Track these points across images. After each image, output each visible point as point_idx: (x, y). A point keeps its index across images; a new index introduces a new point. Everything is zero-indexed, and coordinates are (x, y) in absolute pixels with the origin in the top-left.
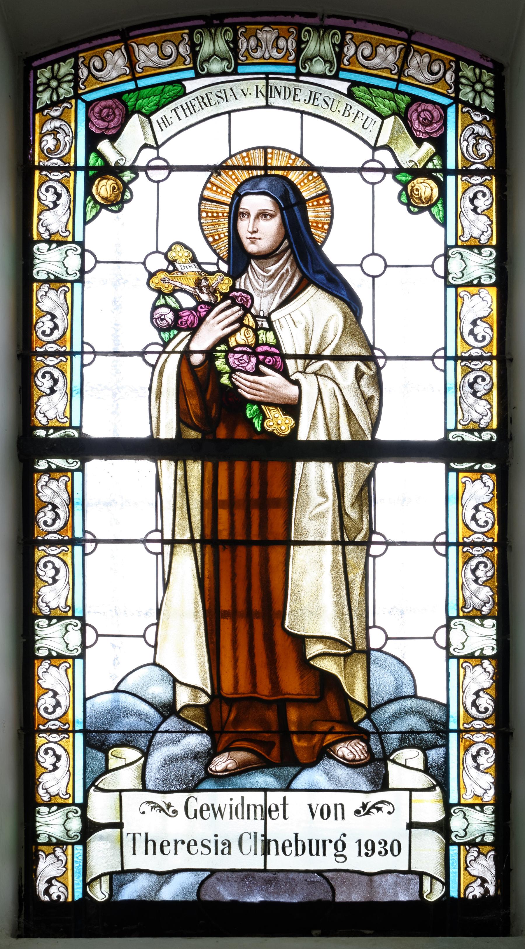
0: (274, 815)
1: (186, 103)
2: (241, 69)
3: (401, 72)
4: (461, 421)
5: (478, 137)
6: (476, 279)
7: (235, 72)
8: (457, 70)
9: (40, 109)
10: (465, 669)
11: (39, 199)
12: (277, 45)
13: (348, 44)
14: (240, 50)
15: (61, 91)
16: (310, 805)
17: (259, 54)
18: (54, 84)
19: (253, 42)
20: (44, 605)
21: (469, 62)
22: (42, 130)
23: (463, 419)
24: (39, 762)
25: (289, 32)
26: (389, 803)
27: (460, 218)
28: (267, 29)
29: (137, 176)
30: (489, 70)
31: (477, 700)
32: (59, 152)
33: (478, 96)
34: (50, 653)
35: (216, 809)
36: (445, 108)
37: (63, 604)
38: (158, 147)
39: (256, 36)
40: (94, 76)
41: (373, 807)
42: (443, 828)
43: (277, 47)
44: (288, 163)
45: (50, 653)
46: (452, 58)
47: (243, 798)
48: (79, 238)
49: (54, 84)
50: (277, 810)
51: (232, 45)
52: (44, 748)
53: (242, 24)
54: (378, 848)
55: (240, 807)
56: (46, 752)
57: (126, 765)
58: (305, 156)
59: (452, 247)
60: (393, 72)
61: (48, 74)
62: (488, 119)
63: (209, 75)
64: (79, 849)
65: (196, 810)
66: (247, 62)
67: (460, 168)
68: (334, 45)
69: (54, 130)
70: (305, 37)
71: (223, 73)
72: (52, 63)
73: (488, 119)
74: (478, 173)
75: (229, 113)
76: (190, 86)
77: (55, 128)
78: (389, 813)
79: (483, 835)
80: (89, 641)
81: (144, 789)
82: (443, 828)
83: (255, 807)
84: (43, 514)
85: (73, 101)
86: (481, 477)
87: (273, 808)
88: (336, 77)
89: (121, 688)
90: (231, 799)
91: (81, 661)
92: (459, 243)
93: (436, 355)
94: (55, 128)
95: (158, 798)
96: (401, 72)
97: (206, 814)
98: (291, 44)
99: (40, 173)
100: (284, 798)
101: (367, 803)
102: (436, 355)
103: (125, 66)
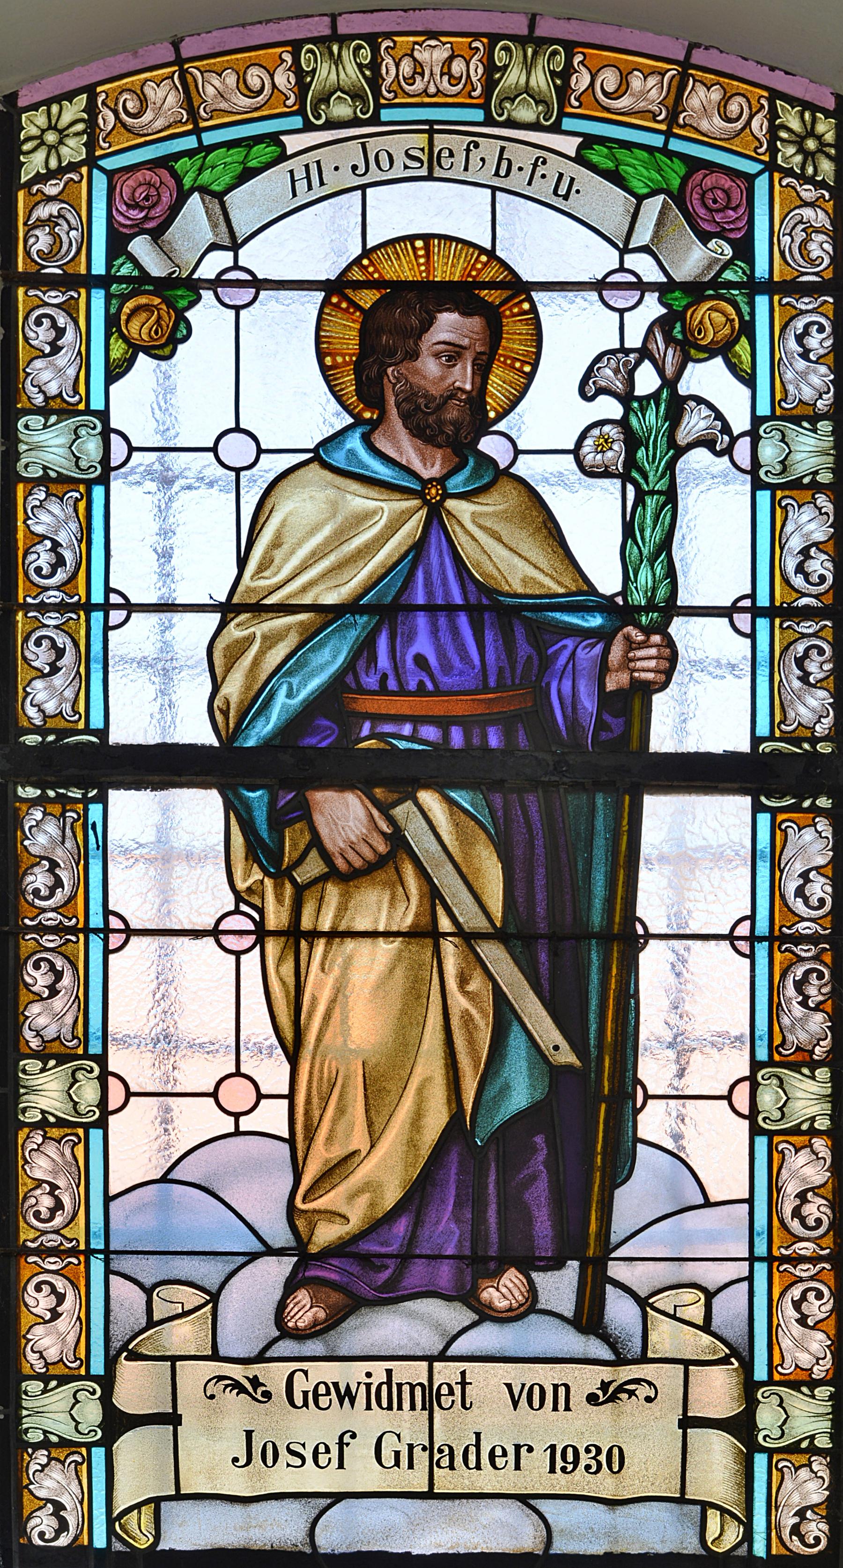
0: (446, 1401)
2: (386, 115)
3: (672, 119)
4: (779, 1368)
5: (810, 230)
6: (806, 1120)
7: (375, 120)
8: (773, 114)
9: (26, 182)
10: (785, 831)
11: (26, 339)
12: (449, 68)
13: (577, 72)
14: (384, 80)
15: (64, 150)
16: (509, 1386)
17: (419, 85)
18: (51, 138)
19: (406, 67)
20: (36, 390)
21: (792, 101)
22: (28, 220)
23: (781, 1365)
24: (26, 1305)
25: (471, 49)
26: (650, 1383)
27: (778, 1017)
28: (433, 43)
29: (199, 298)
30: (827, 114)
31: (806, 564)
32: (58, 257)
33: (810, 161)
34: (46, 474)
36: (750, 179)
37: (66, 1032)
38: (235, 246)
39: (411, 55)
40: (124, 125)
41: (620, 1389)
42: (742, 1427)
43: (451, 76)
44: (469, 275)
45: (46, 474)
46: (765, 94)
47: (389, 1372)
48: (97, 403)
49: (51, 138)
50: (451, 1392)
51: (368, 73)
52: (36, 1280)
53: (388, 35)
54: (584, 1459)
55: (384, 1388)
56: (38, 1288)
57: (185, 1314)
59: (765, 419)
60: (659, 118)
61: (41, 119)
62: (827, 198)
63: (331, 125)
64: (99, 1453)
66: (397, 101)
67: (778, 604)
68: (553, 74)
69: (49, 220)
70: (500, 60)
71: (355, 122)
72: (48, 103)
73: (827, 198)
74: (807, 613)
75: (363, 188)
76: (293, 143)
77: (51, 216)
78: (649, 1399)
79: (816, 473)
80: (117, 457)
81: (215, 1356)
82: (742, 1427)
83: (412, 1387)
84: (35, 556)
85: (84, 170)
86: (813, 497)
87: (445, 1390)
88: (555, 128)
89: (173, 1175)
90: (369, 1375)
91: (100, 1132)
92: (777, 1377)
94: (51, 216)
95: (236, 1372)
96: (672, 119)
97: (324, 1401)
98: (477, 71)
99: (25, 615)
100: (463, 1374)
101: (611, 1382)
103: (181, 107)
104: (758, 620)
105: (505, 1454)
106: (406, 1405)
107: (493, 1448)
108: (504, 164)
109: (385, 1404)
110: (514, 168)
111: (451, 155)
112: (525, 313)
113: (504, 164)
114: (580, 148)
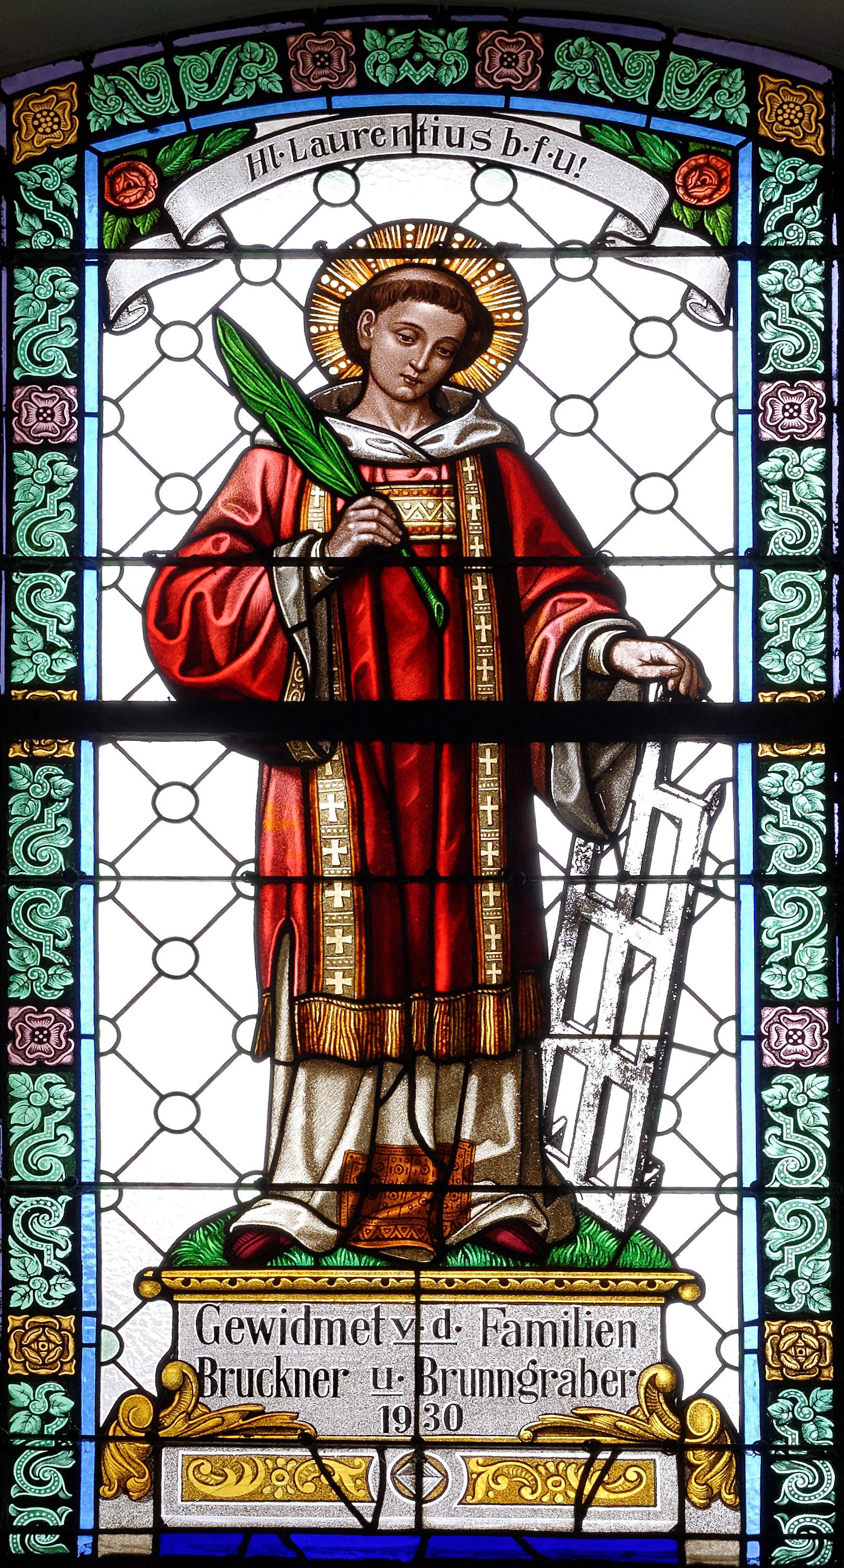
1: (345, 134)
35: (257, 1327)
55: (302, 1325)
58: (531, 311)
65: (217, 1329)
83: (542, 1326)
93: (721, 873)
97: (236, 1334)
102: (721, 873)
104: (741, 571)
105: (611, 1329)
106: (560, 1342)
107: (356, 1322)
108: (513, 145)
109: (302, 1339)
110: (522, 148)
111: (383, 133)
112: (318, 325)
113: (513, 145)
114: (254, 130)
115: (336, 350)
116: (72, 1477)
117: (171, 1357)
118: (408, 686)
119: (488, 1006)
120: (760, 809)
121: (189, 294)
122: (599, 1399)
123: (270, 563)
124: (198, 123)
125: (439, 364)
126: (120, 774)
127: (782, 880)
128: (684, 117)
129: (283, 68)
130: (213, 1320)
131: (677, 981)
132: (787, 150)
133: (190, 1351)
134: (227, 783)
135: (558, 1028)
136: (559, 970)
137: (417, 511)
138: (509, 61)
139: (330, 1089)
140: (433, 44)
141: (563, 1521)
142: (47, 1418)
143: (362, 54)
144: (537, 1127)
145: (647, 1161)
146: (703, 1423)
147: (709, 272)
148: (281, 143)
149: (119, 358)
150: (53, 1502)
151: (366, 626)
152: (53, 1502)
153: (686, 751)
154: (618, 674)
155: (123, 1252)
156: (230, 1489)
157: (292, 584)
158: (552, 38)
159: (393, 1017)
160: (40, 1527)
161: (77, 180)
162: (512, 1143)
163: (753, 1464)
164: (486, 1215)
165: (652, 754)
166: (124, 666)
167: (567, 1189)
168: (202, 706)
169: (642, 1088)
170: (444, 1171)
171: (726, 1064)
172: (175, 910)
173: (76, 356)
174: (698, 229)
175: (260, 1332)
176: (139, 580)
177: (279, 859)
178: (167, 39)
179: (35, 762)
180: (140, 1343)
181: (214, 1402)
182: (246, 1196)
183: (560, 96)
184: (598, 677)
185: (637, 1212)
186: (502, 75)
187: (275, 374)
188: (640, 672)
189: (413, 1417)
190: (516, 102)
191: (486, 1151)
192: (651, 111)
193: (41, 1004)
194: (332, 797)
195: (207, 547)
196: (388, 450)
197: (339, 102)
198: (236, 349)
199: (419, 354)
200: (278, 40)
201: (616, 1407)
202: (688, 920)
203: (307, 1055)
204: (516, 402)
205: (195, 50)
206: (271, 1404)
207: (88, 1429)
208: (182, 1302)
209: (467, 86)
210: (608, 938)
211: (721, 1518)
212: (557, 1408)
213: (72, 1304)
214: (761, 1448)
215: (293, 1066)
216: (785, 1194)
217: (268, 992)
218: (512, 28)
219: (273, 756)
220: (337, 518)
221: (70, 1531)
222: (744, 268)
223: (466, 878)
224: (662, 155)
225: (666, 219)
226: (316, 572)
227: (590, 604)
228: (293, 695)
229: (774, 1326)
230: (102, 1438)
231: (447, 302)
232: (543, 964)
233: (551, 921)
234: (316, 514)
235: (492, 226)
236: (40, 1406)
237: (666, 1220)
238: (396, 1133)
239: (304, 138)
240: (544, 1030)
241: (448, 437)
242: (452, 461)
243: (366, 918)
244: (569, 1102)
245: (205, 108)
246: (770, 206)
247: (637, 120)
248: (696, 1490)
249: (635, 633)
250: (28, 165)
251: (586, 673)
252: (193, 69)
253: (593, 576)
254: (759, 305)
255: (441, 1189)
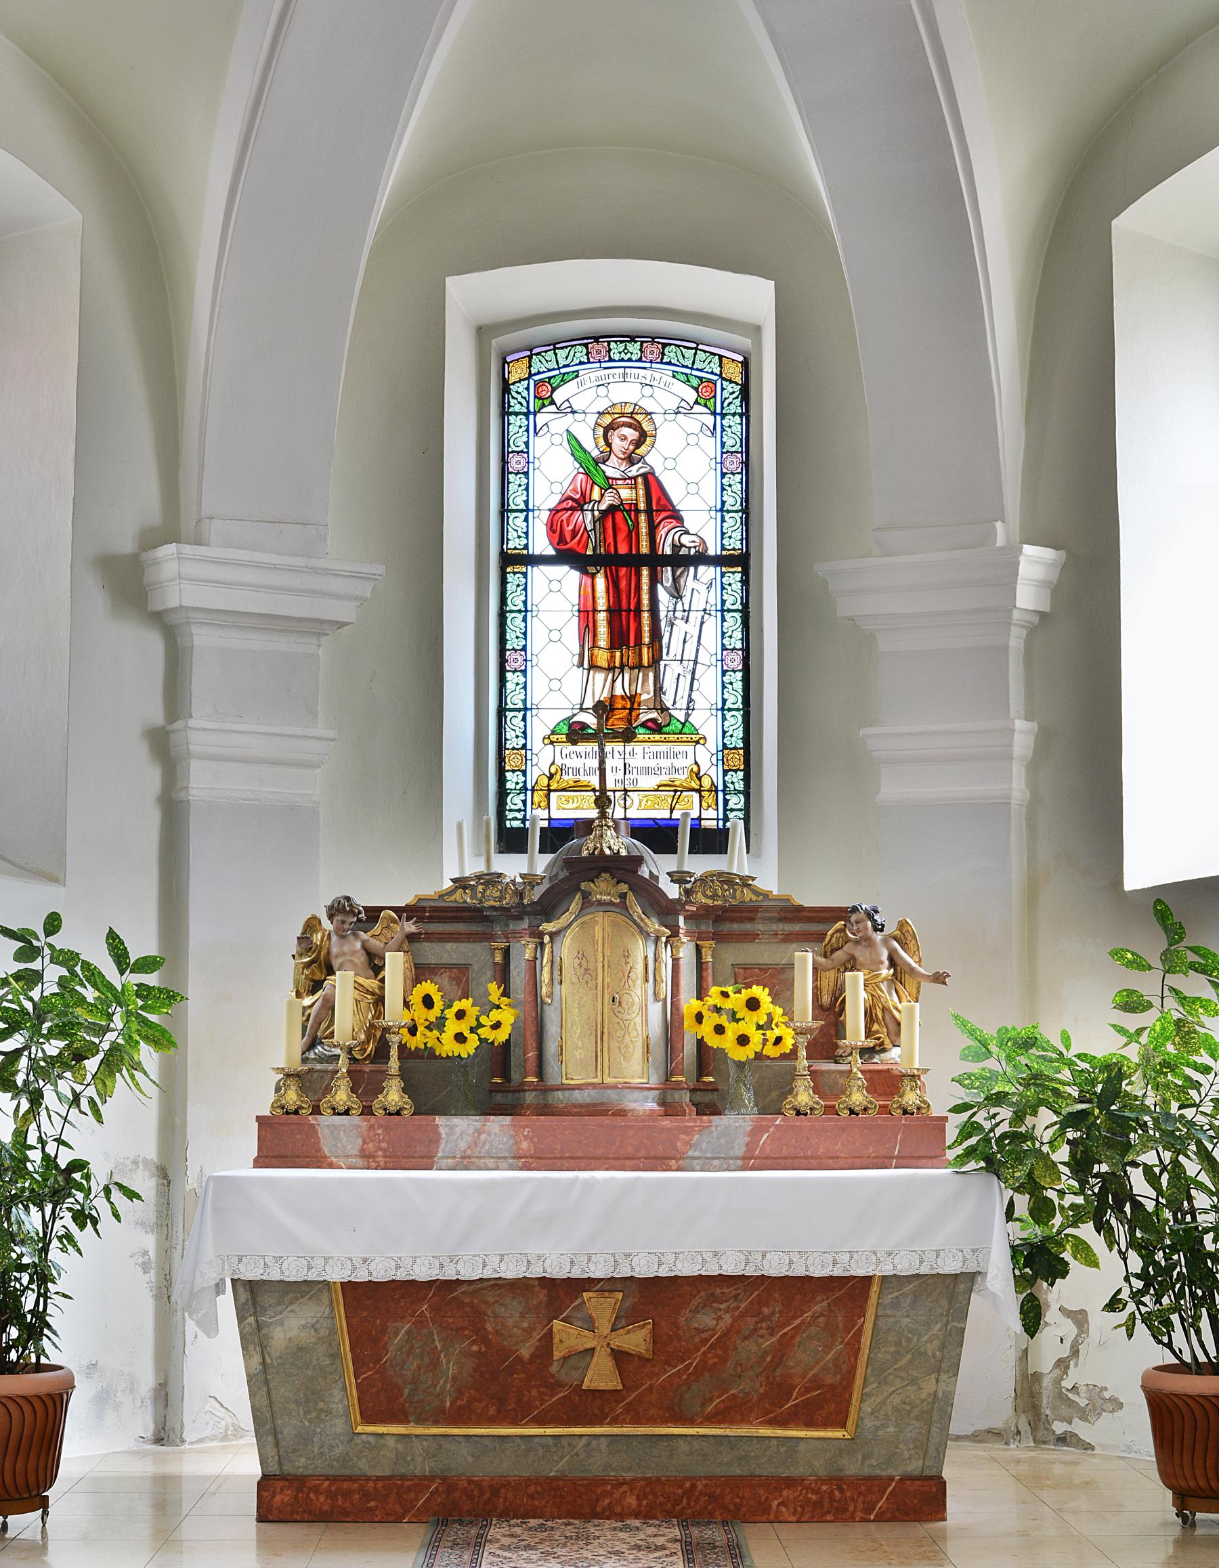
115: (602, 442)
116: (524, 802)
117: (553, 763)
118: (623, 549)
119: (645, 650)
120: (723, 588)
121: (559, 424)
122: (677, 776)
123: (582, 510)
124: (563, 371)
125: (632, 447)
126: (539, 575)
127: (729, 611)
128: (701, 370)
129: (588, 354)
130: (565, 751)
131: (699, 642)
132: (731, 381)
133: (559, 762)
134: (568, 578)
135: (665, 657)
136: (665, 641)
137: (626, 494)
138: (652, 353)
139: (599, 677)
140: (630, 347)
141: (665, 814)
142: (517, 783)
143: (610, 350)
144: (659, 690)
145: (690, 700)
146: (706, 783)
147: (709, 420)
148: (586, 377)
149: (539, 445)
150: (519, 810)
151: (610, 531)
152: (519, 810)
153: (702, 569)
154: (682, 545)
155: (540, 727)
156: (570, 805)
157: (589, 516)
158: (664, 345)
159: (618, 654)
160: (515, 819)
161: (528, 389)
162: (652, 694)
163: (721, 795)
164: (644, 717)
165: (692, 569)
166: (541, 544)
167: (668, 709)
168: (566, 555)
169: (689, 677)
170: (632, 703)
171: (713, 668)
172: (555, 621)
173: (527, 444)
174: (706, 406)
175: (579, 755)
176: (545, 515)
177: (585, 605)
178: (554, 345)
179: (515, 573)
180: (543, 759)
181: (565, 777)
182: (575, 712)
183: (666, 363)
184: (676, 547)
185: (687, 716)
186: (650, 357)
187: (585, 450)
188: (688, 545)
189: (623, 782)
190: (654, 365)
191: (644, 697)
192: (692, 369)
193: (516, 651)
194: (600, 582)
195: (564, 505)
196: (617, 475)
197: (603, 365)
198: (574, 443)
199: (625, 444)
200: (586, 345)
201: (682, 778)
202: (702, 623)
203: (593, 666)
204: (654, 460)
205: (562, 348)
206: (582, 778)
207: (529, 787)
208: (503, 539)
209: (640, 360)
210: (680, 626)
211: (711, 813)
212: (664, 778)
213: (524, 747)
214: (723, 791)
215: (589, 670)
216: (730, 710)
217: (582, 646)
218: (653, 342)
219: (584, 572)
220: (602, 496)
221: (524, 820)
222: (718, 418)
223: (638, 611)
224: (695, 382)
225: (696, 402)
226: (596, 513)
227: (674, 523)
228: (589, 552)
229: (726, 752)
230: (533, 790)
231: (634, 426)
232: (661, 638)
233: (663, 624)
234: (596, 495)
235: (648, 405)
236: (515, 780)
237: (695, 719)
238: (618, 691)
239: (593, 376)
240: (661, 658)
241: (634, 471)
242: (635, 478)
243: (610, 623)
244: (668, 684)
245: (565, 366)
246: (869, 1395)
247: (688, 371)
248: (704, 805)
249: (687, 533)
250: (513, 384)
251: (673, 545)
252: (562, 354)
253: (676, 516)
254: (723, 430)
255: (632, 709)
